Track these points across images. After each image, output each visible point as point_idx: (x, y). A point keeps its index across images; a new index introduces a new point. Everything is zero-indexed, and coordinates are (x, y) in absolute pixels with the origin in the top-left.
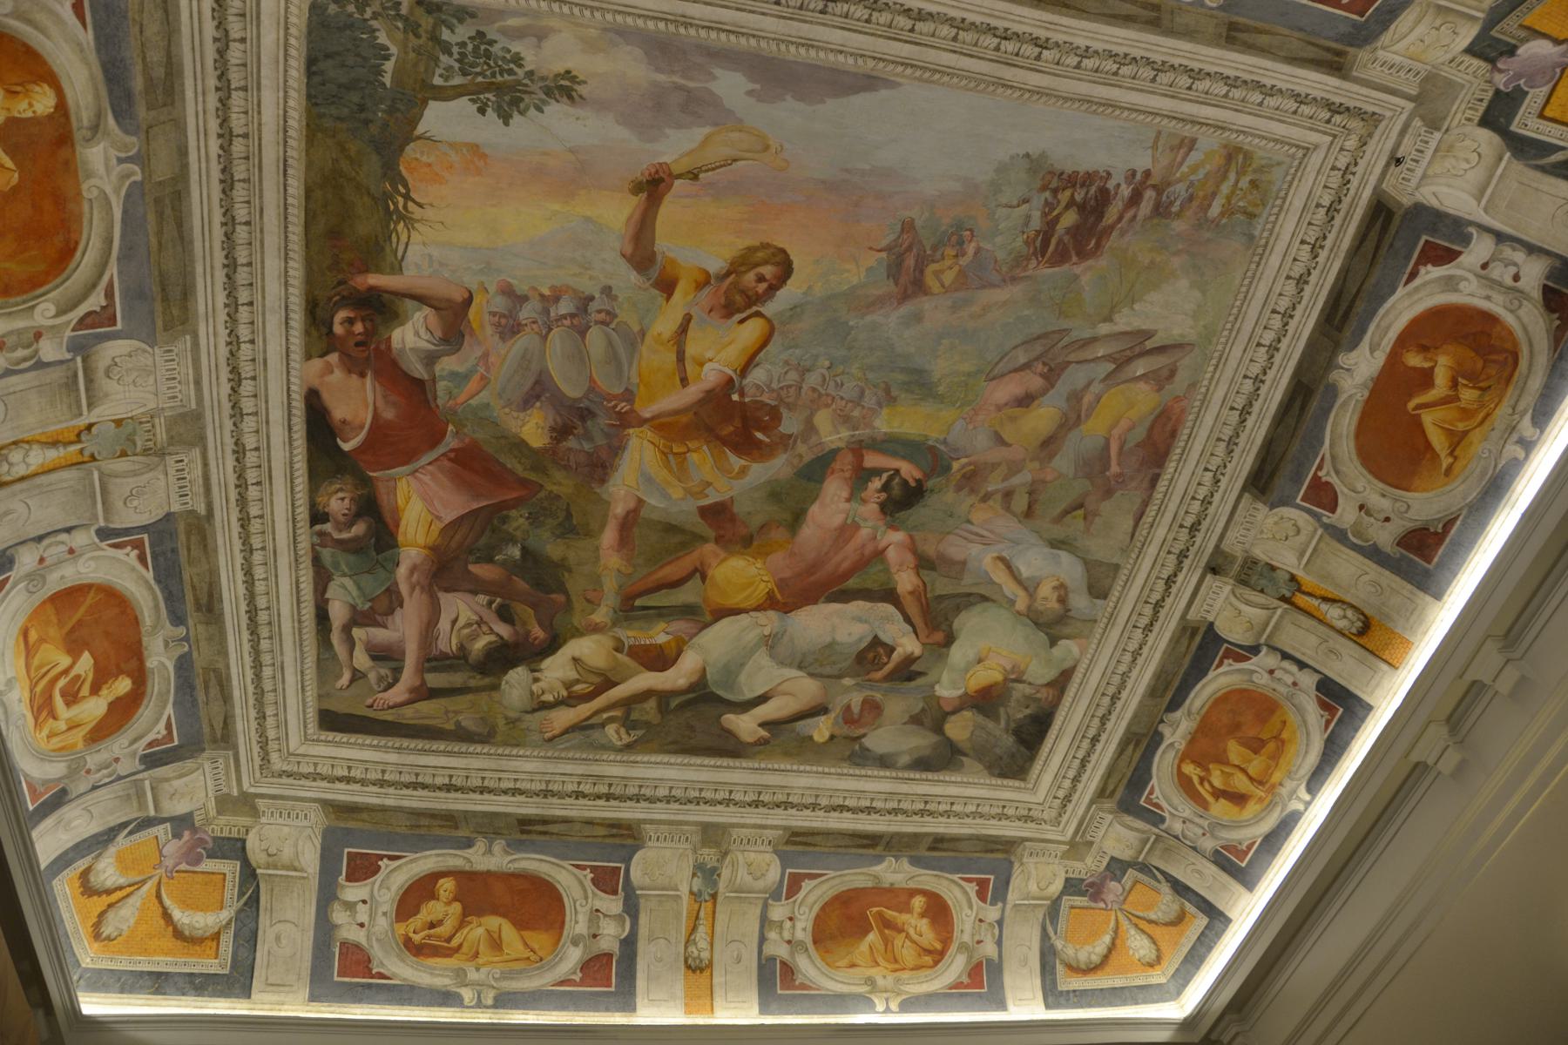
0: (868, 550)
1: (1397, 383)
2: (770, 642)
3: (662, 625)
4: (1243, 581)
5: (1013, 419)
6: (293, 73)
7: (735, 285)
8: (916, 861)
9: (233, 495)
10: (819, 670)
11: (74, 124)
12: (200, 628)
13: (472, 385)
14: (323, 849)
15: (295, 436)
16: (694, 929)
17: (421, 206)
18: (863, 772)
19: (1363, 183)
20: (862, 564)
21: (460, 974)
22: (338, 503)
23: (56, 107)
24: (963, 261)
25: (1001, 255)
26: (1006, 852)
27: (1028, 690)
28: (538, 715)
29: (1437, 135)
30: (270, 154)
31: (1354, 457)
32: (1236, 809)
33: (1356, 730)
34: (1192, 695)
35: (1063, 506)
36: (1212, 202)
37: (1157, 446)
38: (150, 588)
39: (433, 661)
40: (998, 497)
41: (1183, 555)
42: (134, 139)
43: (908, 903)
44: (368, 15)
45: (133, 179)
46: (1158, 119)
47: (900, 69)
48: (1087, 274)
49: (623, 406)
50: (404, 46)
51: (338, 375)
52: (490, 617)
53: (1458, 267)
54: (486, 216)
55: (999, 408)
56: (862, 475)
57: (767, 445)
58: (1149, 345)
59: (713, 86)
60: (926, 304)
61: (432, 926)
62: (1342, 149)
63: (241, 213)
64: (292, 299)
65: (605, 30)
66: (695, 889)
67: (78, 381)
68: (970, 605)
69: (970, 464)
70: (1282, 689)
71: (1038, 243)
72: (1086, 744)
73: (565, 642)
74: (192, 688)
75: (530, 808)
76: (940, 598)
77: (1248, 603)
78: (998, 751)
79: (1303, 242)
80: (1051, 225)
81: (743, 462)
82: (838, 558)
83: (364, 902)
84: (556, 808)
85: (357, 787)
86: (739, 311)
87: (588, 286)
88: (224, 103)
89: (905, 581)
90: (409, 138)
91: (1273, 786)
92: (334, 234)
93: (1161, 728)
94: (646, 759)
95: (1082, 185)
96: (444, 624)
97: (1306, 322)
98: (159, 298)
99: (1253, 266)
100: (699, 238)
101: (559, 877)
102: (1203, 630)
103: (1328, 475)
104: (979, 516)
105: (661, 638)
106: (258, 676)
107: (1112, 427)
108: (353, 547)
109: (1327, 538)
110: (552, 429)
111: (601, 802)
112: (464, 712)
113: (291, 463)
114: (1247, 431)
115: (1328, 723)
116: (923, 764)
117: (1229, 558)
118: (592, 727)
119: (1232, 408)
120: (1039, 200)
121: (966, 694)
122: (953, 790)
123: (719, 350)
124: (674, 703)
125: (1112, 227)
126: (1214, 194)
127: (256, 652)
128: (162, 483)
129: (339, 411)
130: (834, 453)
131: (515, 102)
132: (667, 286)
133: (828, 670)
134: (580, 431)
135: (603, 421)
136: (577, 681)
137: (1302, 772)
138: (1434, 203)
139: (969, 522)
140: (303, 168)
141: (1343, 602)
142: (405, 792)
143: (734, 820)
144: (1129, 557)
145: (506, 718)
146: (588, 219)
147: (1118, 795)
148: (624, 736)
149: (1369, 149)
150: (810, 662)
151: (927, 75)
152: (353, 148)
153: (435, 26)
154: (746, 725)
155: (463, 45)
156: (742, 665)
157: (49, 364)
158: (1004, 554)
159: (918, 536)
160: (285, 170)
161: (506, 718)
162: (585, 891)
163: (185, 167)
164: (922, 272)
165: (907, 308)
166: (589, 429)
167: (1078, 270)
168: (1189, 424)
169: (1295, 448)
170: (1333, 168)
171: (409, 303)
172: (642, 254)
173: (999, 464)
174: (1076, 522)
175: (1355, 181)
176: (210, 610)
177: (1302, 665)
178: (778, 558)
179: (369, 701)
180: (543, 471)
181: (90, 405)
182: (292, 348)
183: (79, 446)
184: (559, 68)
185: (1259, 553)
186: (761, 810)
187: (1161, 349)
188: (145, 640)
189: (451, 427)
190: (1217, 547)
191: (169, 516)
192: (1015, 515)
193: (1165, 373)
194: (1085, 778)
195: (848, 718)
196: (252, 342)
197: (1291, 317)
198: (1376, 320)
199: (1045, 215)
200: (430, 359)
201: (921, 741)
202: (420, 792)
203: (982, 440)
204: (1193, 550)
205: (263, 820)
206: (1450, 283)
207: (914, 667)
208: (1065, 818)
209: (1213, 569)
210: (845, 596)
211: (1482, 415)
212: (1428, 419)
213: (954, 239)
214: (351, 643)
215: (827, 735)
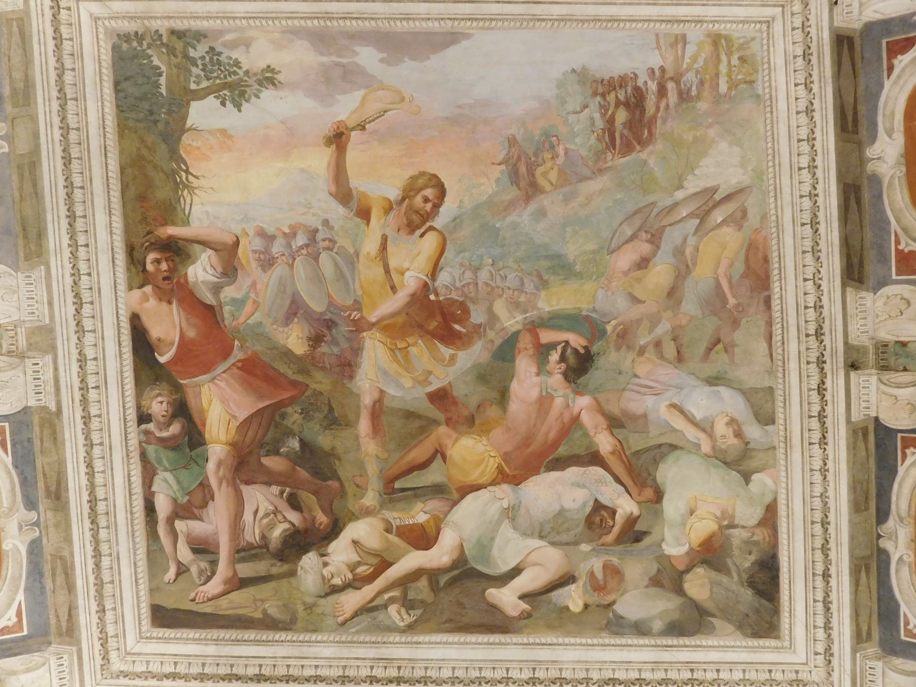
0: (567, 417)
3: (419, 505)
4: (884, 368)
5: (639, 280)
7: (410, 207)
9: (78, 396)
10: (557, 539)
13: (248, 308)
17: (197, 177)
19: (819, 29)
22: (158, 406)
24: (560, 161)
25: (584, 153)
27: (745, 534)
28: (330, 598)
30: (95, 143)
34: (894, 498)
35: (703, 346)
37: (758, 274)
38: (9, 473)
39: (245, 552)
40: (651, 348)
44: (145, 47)
46: (652, 25)
47: (469, 23)
48: (650, 156)
49: (355, 315)
50: (169, 65)
51: (152, 302)
52: (283, 506)
55: (626, 274)
56: (542, 351)
57: (465, 335)
58: (718, 197)
59: (357, 59)
60: (544, 201)
62: (793, 14)
63: (77, 180)
64: (116, 244)
68: (663, 456)
73: (344, 526)
74: (41, 575)
76: (637, 453)
77: (899, 386)
78: (742, 608)
79: (796, 85)
80: (611, 121)
81: (451, 351)
82: (544, 429)
86: (418, 227)
88: (63, 107)
89: (605, 443)
90: (183, 131)
92: (142, 198)
95: (621, 87)
96: (248, 516)
98: (21, 235)
99: (769, 115)
100: (380, 177)
104: (642, 369)
105: (422, 518)
106: (98, 565)
110: (309, 339)
113: (122, 372)
116: (676, 629)
119: (803, 224)
121: (691, 549)
122: (714, 656)
123: (412, 259)
125: (654, 118)
126: (717, 75)
129: (155, 331)
130: (516, 334)
131: (242, 94)
132: (365, 214)
133: (565, 538)
134: (328, 338)
138: (878, 17)
139: (636, 376)
140: (117, 152)
144: (776, 377)
145: (304, 604)
146: (303, 170)
148: (405, 616)
150: (550, 530)
152: (150, 139)
153: (185, 47)
154: (507, 598)
155: (203, 58)
156: (493, 539)
158: (675, 401)
159: (601, 397)
160: (106, 154)
163: (38, 146)
164: (533, 175)
165: (532, 207)
166: (334, 333)
167: (644, 155)
168: (775, 248)
169: (869, 235)
170: (793, 29)
171: (197, 247)
172: (343, 193)
174: (720, 359)
175: (813, 31)
178: (497, 433)
179: (193, 595)
182: (119, 281)
184: (262, 65)
185: (886, 334)
187: (728, 198)
189: (236, 343)
190: (846, 343)
191: (26, 410)
193: (739, 214)
196: (89, 274)
197: (814, 139)
199: (603, 115)
200: (216, 289)
203: (621, 302)
204: (827, 354)
207: (638, 527)
209: (853, 366)
210: (559, 464)
213: (547, 145)
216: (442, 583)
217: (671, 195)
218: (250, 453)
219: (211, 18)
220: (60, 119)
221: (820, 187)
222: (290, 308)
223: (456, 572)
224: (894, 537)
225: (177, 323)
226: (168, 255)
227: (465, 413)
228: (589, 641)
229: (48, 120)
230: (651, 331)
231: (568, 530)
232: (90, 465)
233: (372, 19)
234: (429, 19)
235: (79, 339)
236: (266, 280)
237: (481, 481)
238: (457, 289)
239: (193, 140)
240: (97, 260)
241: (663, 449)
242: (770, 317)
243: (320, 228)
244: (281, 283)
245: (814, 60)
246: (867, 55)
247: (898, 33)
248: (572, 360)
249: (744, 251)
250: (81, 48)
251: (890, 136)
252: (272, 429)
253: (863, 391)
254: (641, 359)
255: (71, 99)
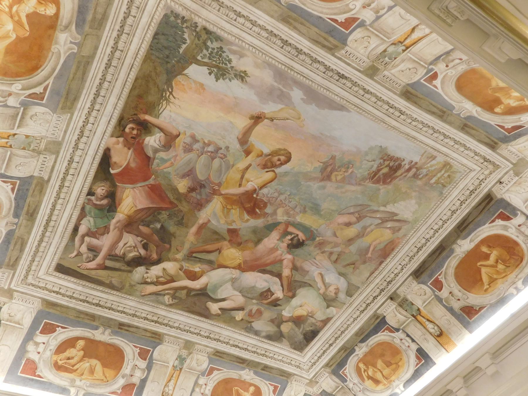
1: (475, 256)
2: (233, 281)
3: (199, 265)
7: (270, 159)
8: (256, 373)
9: (61, 176)
10: (246, 295)
11: (59, 23)
12: (24, 221)
15: (94, 162)
16: (170, 380)
17: (174, 98)
18: (248, 335)
19: (486, 186)
20: (273, 263)
21: (73, 381)
22: (101, 190)
24: (346, 174)
25: (359, 176)
26: (287, 377)
27: (314, 321)
28: (142, 285)
29: (517, 178)
30: (128, 61)
32: (375, 385)
33: (428, 370)
35: (348, 262)
36: (432, 178)
37: (385, 252)
38: (11, 201)
39: (111, 256)
40: (328, 253)
41: (382, 290)
42: (80, 37)
43: (248, 389)
45: (73, 51)
46: (427, 147)
47: (353, 107)
48: (383, 189)
49: (216, 188)
50: (192, 43)
51: (120, 146)
53: (510, 223)
54: (197, 110)
55: (339, 224)
56: (286, 233)
57: (259, 214)
58: (395, 218)
60: (328, 184)
61: (69, 359)
62: (483, 173)
63: (109, 77)
64: (115, 114)
66: (175, 365)
67: (19, 116)
69: (322, 240)
70: (403, 347)
71: (372, 175)
72: (327, 346)
73: (163, 262)
74: (9, 243)
76: (296, 281)
77: (400, 313)
78: (296, 339)
80: (379, 170)
81: (248, 218)
83: (44, 343)
84: (135, 322)
86: (268, 168)
88: (119, 36)
89: (286, 272)
90: (180, 73)
91: (391, 381)
92: (140, 97)
93: (356, 348)
94: (175, 311)
95: (394, 161)
96: (121, 244)
97: (451, 226)
99: (439, 203)
100: (264, 140)
101: (126, 349)
102: (381, 318)
103: (442, 278)
105: (197, 269)
106: (39, 245)
108: (100, 208)
109: (435, 300)
112: (115, 278)
114: (418, 255)
116: (269, 337)
117: (398, 296)
118: (160, 295)
119: (416, 247)
120: (378, 162)
122: (276, 350)
123: (255, 179)
124: (193, 293)
126: (435, 176)
127: (43, 235)
128: (35, 164)
129: (115, 158)
130: (279, 223)
131: (223, 75)
132: (248, 153)
133: (249, 296)
135: (207, 190)
136: (162, 277)
138: (509, 200)
139: (315, 259)
140: (138, 69)
141: (435, 323)
143: (198, 342)
145: (130, 284)
146: (231, 122)
147: (333, 367)
148: (170, 301)
149: (492, 176)
150: (244, 292)
151: (361, 111)
152: (159, 69)
154: (214, 308)
155: (213, 49)
156: (221, 286)
158: (322, 273)
160: (131, 68)
161: (130, 284)
162: (134, 356)
163: (95, 54)
164: (331, 173)
165: (322, 184)
166: (201, 191)
167: (381, 187)
168: (399, 248)
169: (433, 266)
170: (477, 179)
171: (157, 130)
172: (244, 140)
174: (350, 269)
175: (483, 185)
176: (32, 215)
177: (413, 341)
178: (247, 253)
179: (80, 265)
182: (107, 131)
183: (7, 140)
184: (243, 69)
185: (409, 297)
186: (209, 340)
187: (398, 221)
189: (153, 176)
190: (395, 291)
191: (32, 177)
192: (331, 261)
193: (397, 229)
194: (323, 357)
195: (250, 314)
196: (93, 124)
198: (475, 232)
199: (378, 167)
200: (156, 151)
201: (271, 329)
202: (85, 304)
203: (329, 233)
206: (506, 228)
208: (311, 370)
209: (391, 298)
210: (264, 272)
212: (484, 270)
213: (347, 166)
214: (82, 241)
215: (241, 318)
217: (379, 207)
219: (231, 34)
220: (114, 42)
221: (433, 239)
224: (361, 348)
225: (128, 159)
227: (239, 241)
229: (107, 41)
231: (252, 294)
232: (54, 206)
233: (312, 81)
234: (337, 95)
235: (73, 151)
237: (229, 266)
238: (268, 197)
239: (183, 80)
240: (100, 119)
243: (223, 148)
244: (189, 162)
248: (295, 242)
249: (388, 242)
250: (145, 6)
252: (151, 217)
253: (388, 307)
255: (125, 33)
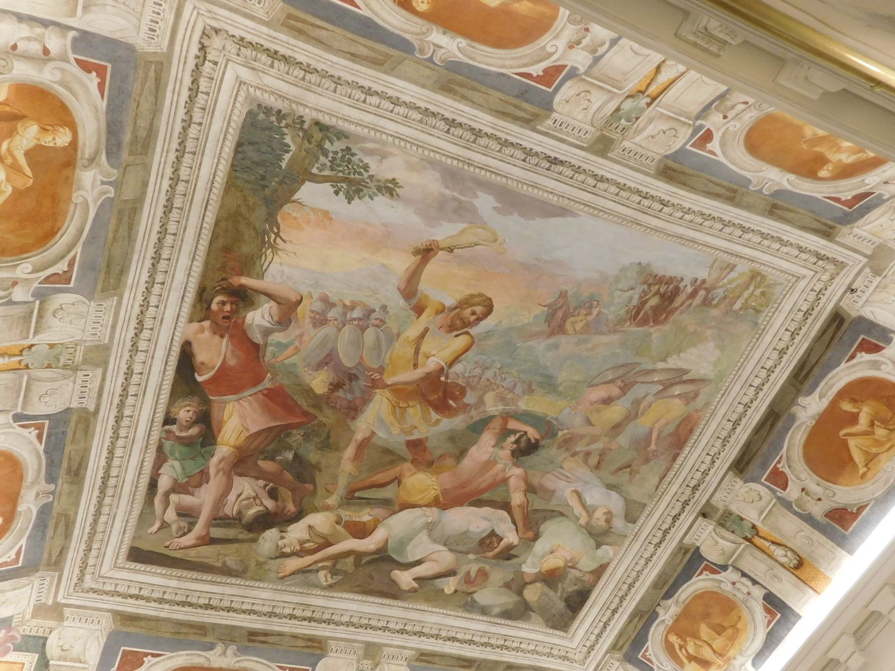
0: (500, 476)
1: (833, 421)
2: (430, 527)
3: (368, 510)
4: (721, 524)
6: (226, 149)
7: (458, 315)
9: (116, 401)
10: (456, 548)
12: (66, 486)
13: (289, 351)
14: (105, 647)
15: (168, 368)
17: (284, 241)
18: (470, 616)
19: (829, 300)
20: (494, 485)
22: (185, 412)
23: (70, 144)
24: (590, 318)
25: (611, 317)
27: (577, 573)
28: (278, 560)
29: (878, 279)
30: (200, 195)
31: (802, 459)
34: (680, 590)
35: (619, 465)
36: (736, 302)
37: (680, 437)
38: (39, 457)
39: (219, 520)
40: (582, 455)
41: (686, 503)
42: (115, 171)
44: (282, 125)
45: (108, 195)
47: (582, 207)
48: (656, 333)
49: (376, 376)
50: (300, 148)
51: (207, 334)
55: (592, 403)
56: (505, 433)
57: (455, 409)
58: (685, 377)
60: (563, 339)
62: (819, 280)
63: (172, 227)
64: (190, 284)
65: (422, 159)
67: (33, 316)
69: (569, 434)
70: (739, 595)
73: (306, 515)
74: (45, 526)
75: (258, 624)
77: (723, 538)
79: (787, 330)
80: (643, 303)
81: (438, 417)
84: (276, 625)
85: (142, 602)
86: (456, 330)
87: (374, 304)
89: (517, 499)
90: (288, 201)
91: (729, 659)
92: (227, 250)
93: (658, 609)
94: (340, 595)
95: (667, 283)
96: (232, 497)
97: (782, 376)
98: (104, 271)
99: (755, 340)
100: (443, 286)
102: (692, 551)
103: (783, 467)
105: (366, 518)
106: (95, 522)
107: (656, 422)
109: (779, 505)
111: (305, 623)
112: (230, 556)
113: (161, 385)
115: (769, 622)
116: (507, 615)
117: (715, 509)
118: (310, 571)
119: (729, 420)
120: (639, 290)
121: (540, 572)
123: (439, 351)
125: (676, 309)
126: (739, 297)
127: (100, 504)
128: (70, 388)
129: (201, 356)
130: (491, 418)
131: (358, 191)
132: (419, 310)
133: (461, 548)
134: (347, 387)
135: (362, 383)
136: (308, 541)
137: (749, 652)
139: (562, 467)
141: (786, 547)
142: (176, 608)
143: (387, 642)
144: (653, 500)
145: (257, 561)
146: (384, 265)
147: (625, 650)
149: (835, 282)
151: (596, 212)
152: (251, 200)
154: (405, 579)
155: (336, 153)
156: (411, 540)
157: (16, 303)
158: (579, 489)
159: (530, 472)
160: (206, 207)
161: (257, 561)
163: (144, 193)
164: (565, 321)
165: (552, 340)
166: (352, 386)
167: (652, 330)
168: (702, 426)
169: (765, 448)
170: (812, 290)
172: (409, 289)
173: (585, 436)
174: (624, 476)
175: (822, 302)
176: (77, 474)
177: (755, 582)
178: (446, 477)
179: (167, 543)
180: (320, 409)
181: (36, 332)
182: (182, 314)
183: (19, 358)
185: (734, 508)
186: (405, 636)
187: (692, 381)
188: (23, 491)
189: (269, 375)
190: (708, 501)
192: (589, 467)
193: (692, 395)
194: (604, 635)
195: (468, 580)
196: (157, 307)
197: (773, 372)
199: (641, 297)
200: (267, 332)
201: (508, 599)
202: (187, 609)
203: (578, 421)
205: (66, 623)
206: (876, 365)
208: (589, 660)
209: (704, 515)
210: (479, 503)
211: (888, 445)
212: (852, 443)
213: (587, 305)
215: (453, 589)
216: (363, 562)
217: (655, 363)
218: (251, 456)
220: (173, 170)
221: (755, 403)
222: (325, 358)
223: (376, 556)
226: (233, 300)
227: (429, 457)
228: (448, 613)
230: (588, 445)
231: (465, 544)
232: (111, 452)
235: (131, 356)
236: (312, 334)
237: (418, 503)
241: (554, 514)
242: (672, 466)
244: (324, 341)
245: (810, 321)
246: (845, 338)
247: (874, 337)
248: (523, 444)
249: (680, 420)
251: (820, 398)
252: (276, 442)
253: (700, 530)
254: (572, 459)
